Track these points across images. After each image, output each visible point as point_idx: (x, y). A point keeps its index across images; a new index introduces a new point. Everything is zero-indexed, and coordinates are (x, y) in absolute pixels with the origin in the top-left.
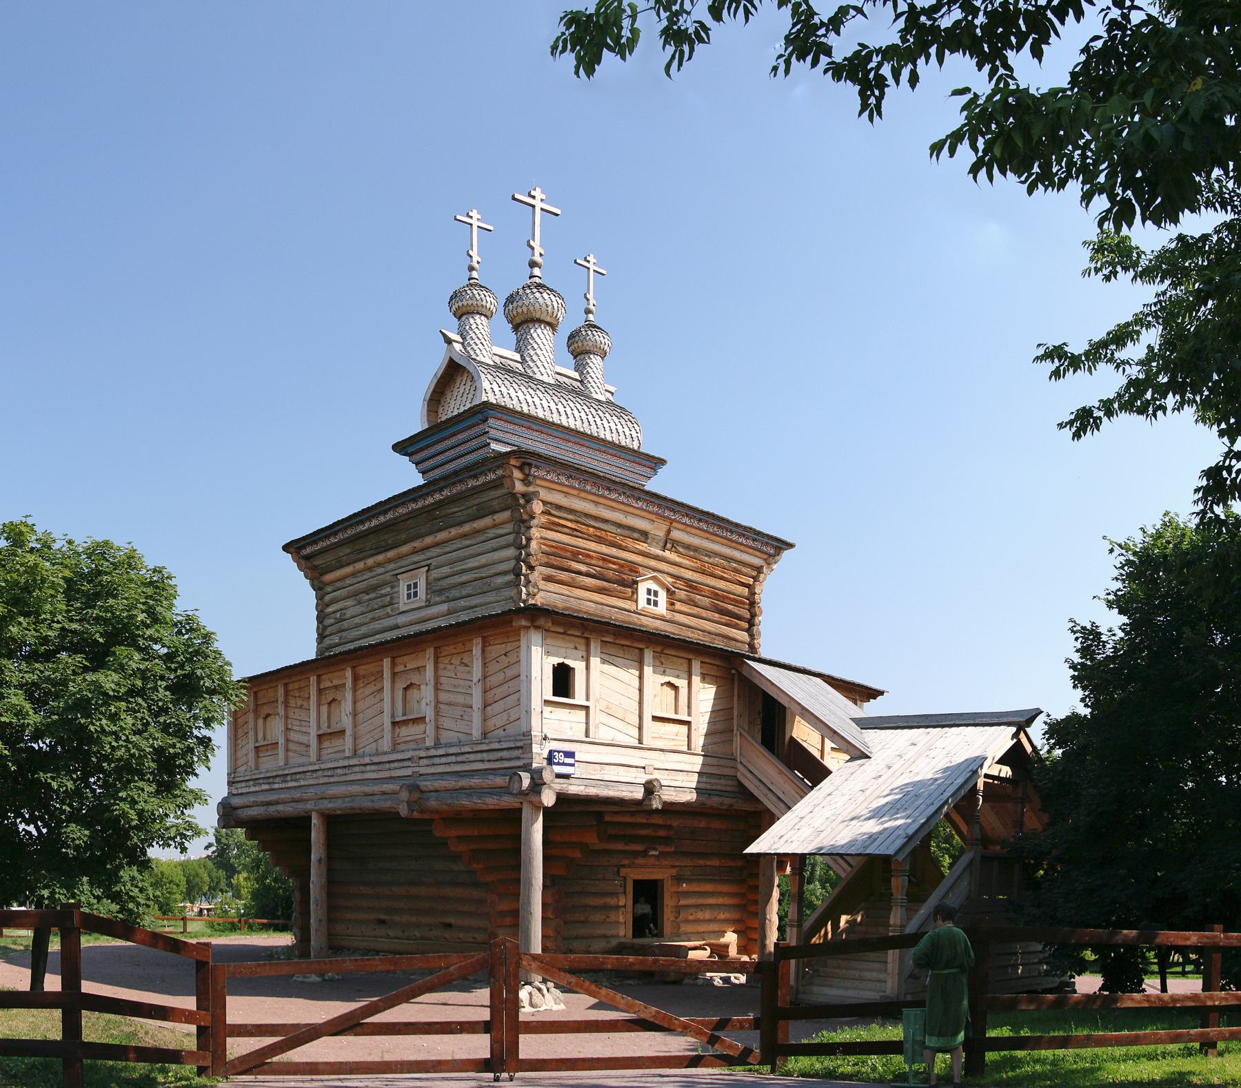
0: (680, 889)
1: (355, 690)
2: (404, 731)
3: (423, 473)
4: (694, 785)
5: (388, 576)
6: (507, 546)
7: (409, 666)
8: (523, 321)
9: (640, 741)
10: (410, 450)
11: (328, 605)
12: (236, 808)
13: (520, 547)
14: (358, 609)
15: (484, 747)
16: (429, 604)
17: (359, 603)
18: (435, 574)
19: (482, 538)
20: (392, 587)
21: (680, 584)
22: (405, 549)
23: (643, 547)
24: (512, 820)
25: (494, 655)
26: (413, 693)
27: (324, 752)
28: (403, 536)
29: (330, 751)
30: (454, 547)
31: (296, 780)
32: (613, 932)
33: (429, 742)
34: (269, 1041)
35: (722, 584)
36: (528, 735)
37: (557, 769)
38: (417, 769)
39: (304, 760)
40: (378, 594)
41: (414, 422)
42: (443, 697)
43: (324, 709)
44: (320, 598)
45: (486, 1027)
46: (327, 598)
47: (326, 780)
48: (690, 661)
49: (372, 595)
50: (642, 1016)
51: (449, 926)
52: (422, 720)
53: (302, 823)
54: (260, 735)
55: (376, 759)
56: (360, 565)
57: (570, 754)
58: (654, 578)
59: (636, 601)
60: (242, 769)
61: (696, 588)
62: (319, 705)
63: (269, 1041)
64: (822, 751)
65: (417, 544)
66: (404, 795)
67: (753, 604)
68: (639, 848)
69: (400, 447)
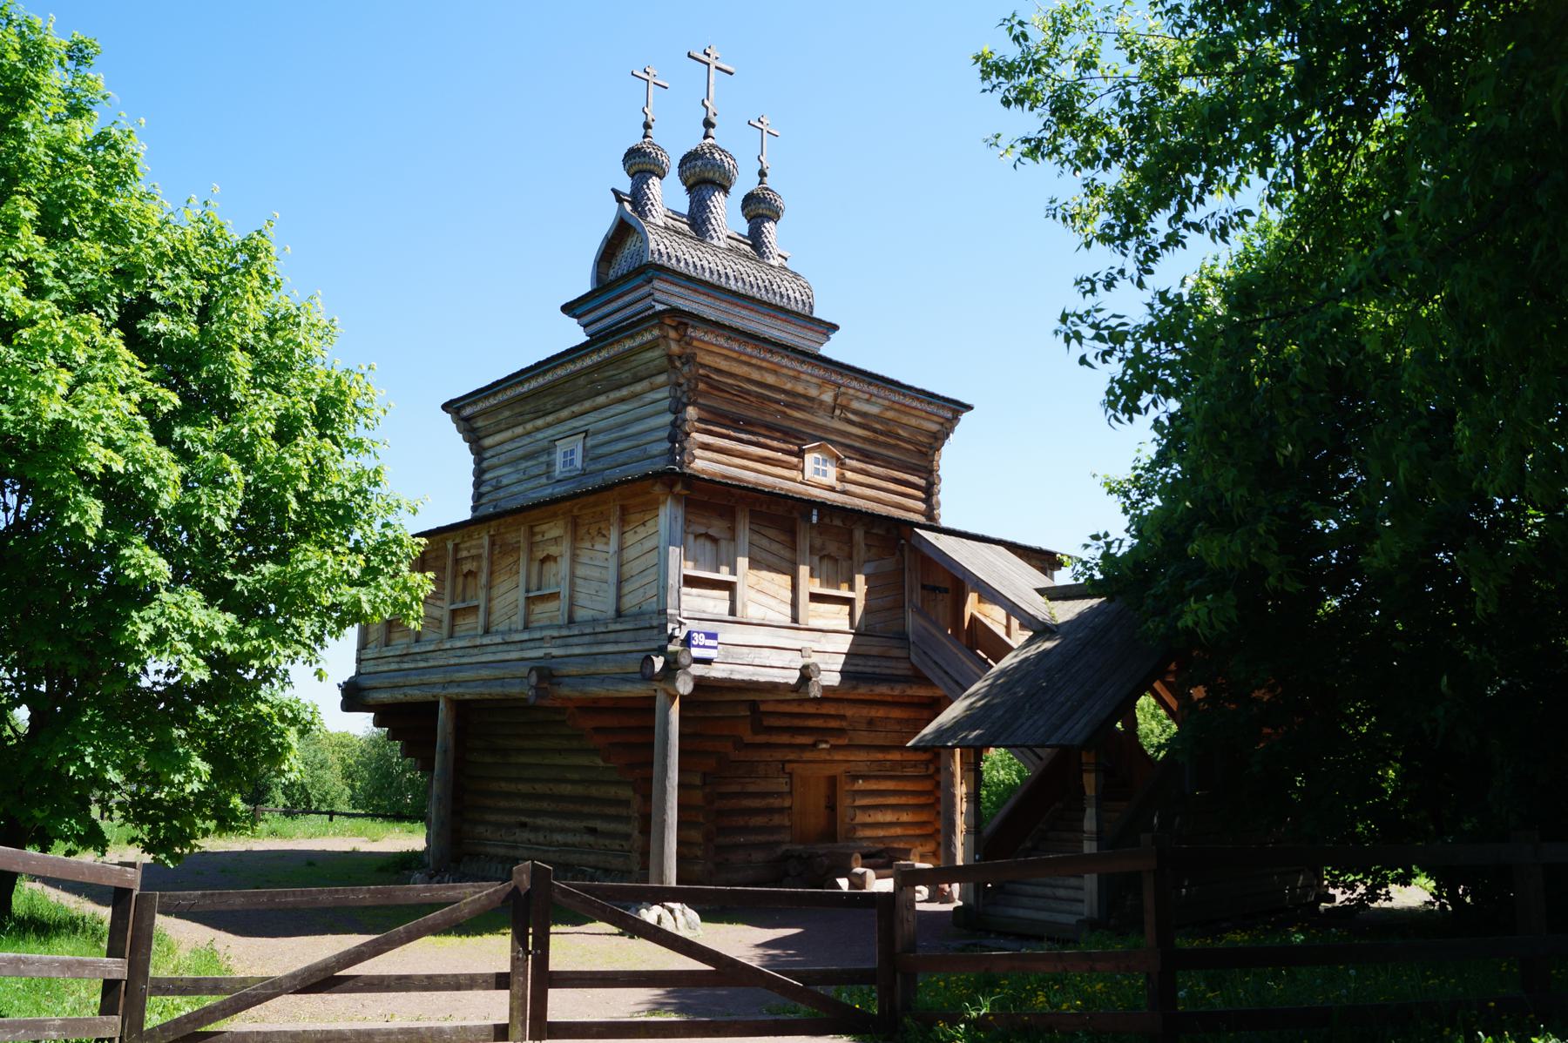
0: (856, 787)
1: (491, 563)
2: (539, 608)
4: (839, 668)
5: (545, 443)
9: (795, 619)
10: (578, 312)
14: (514, 478)
15: (618, 627)
17: (517, 471)
18: (590, 442)
20: (549, 454)
22: (565, 413)
26: (550, 568)
30: (612, 412)
31: (426, 660)
37: (695, 652)
41: (582, 285)
44: (478, 462)
45: (501, 981)
46: (485, 464)
47: (457, 661)
51: (592, 831)
52: (554, 596)
53: (430, 708)
56: (519, 430)
57: (713, 636)
59: (803, 471)
60: (372, 645)
62: (455, 577)
65: (576, 408)
69: (568, 309)
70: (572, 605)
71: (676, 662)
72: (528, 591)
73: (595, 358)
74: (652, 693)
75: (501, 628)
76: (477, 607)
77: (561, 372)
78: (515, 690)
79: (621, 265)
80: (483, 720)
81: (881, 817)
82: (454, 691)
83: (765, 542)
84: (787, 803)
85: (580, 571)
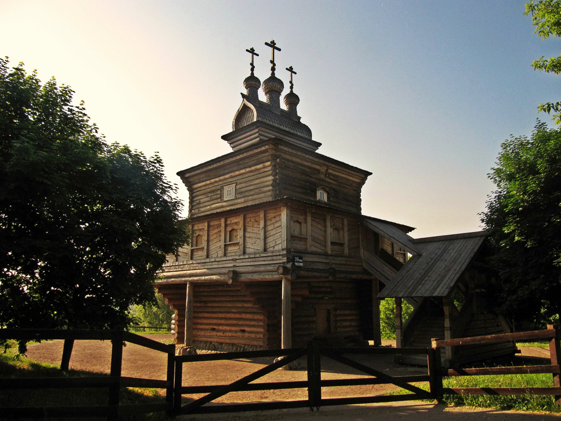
3: (233, 147)
6: (269, 175)
14: (207, 199)
15: (265, 255)
16: (236, 199)
17: (207, 197)
18: (238, 187)
22: (227, 176)
34: (202, 395)
40: (217, 193)
41: (229, 129)
46: (194, 195)
48: (343, 220)
50: (230, 351)
51: (243, 331)
53: (182, 286)
55: (217, 260)
56: (208, 182)
63: (202, 395)
65: (232, 174)
68: (320, 296)
69: (224, 137)
70: (244, 247)
72: (225, 242)
74: (280, 279)
76: (203, 248)
81: (344, 324)
83: (316, 224)
84: (314, 319)
85: (247, 235)
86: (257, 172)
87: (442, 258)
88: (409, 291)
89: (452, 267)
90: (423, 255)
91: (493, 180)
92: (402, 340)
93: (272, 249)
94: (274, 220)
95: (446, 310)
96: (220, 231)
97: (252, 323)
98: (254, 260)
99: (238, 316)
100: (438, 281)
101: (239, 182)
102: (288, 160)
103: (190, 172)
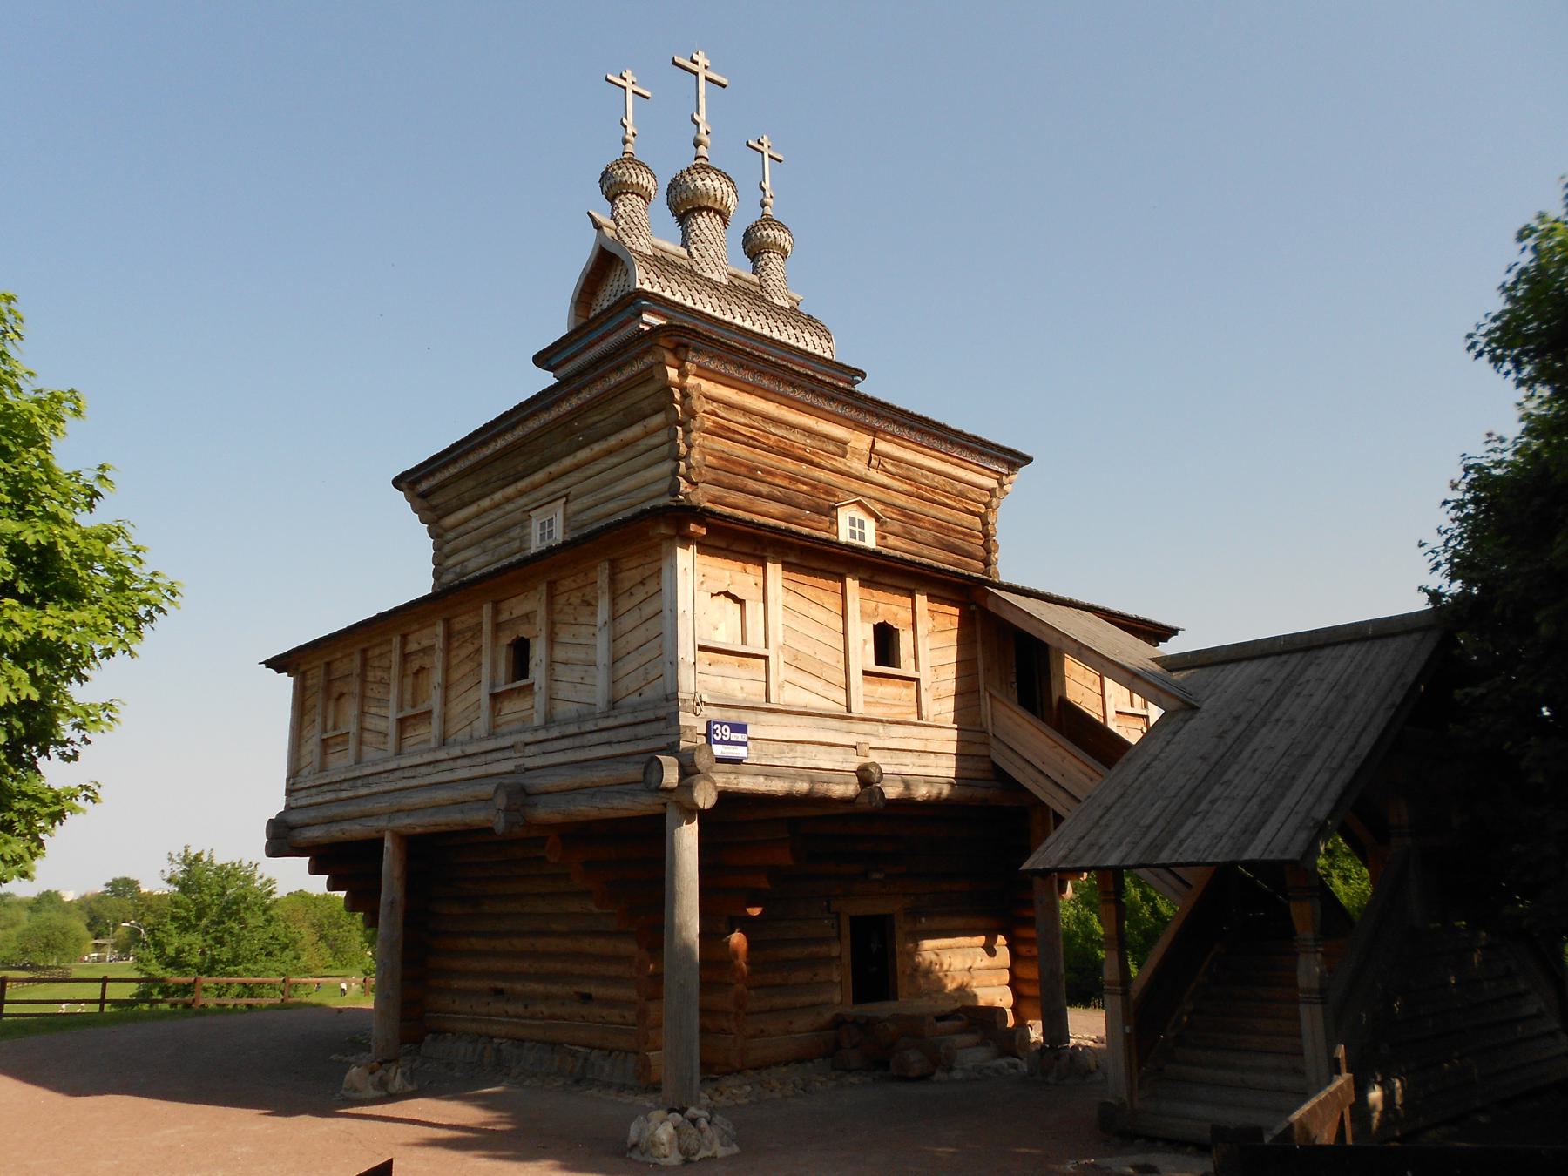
5: (518, 515)
7: (516, 613)
8: (686, 206)
10: (554, 362)
11: (448, 557)
12: (293, 828)
13: (677, 459)
18: (573, 507)
19: (632, 454)
20: (523, 527)
21: (890, 512)
22: (539, 477)
23: (837, 463)
24: (649, 839)
25: (627, 585)
27: (407, 743)
28: (536, 459)
29: (413, 741)
32: (823, 998)
33: (538, 720)
35: (944, 513)
36: (672, 697)
37: (718, 750)
38: (521, 761)
39: (380, 755)
42: (560, 654)
43: (409, 681)
44: (437, 548)
46: (447, 548)
49: (500, 541)
51: (586, 998)
53: (375, 845)
54: (330, 724)
55: (470, 750)
56: (486, 503)
57: (741, 728)
58: (859, 503)
60: (305, 772)
61: (912, 517)
62: (403, 676)
64: (1105, 717)
65: (553, 468)
66: (501, 801)
67: (987, 536)
69: (542, 359)
71: (693, 763)
73: (575, 402)
74: (659, 809)
75: (460, 737)
76: (429, 713)
77: (533, 424)
78: (477, 817)
79: (604, 301)
80: (430, 853)
82: (404, 822)
83: (802, 605)
86: (629, 453)
87: (1277, 714)
88: (1145, 842)
89: (1317, 746)
90: (1205, 706)
91: (1486, 357)
92: (1127, 1037)
93: (635, 698)
94: (640, 594)
95: (1303, 915)
96: (478, 651)
97: (613, 970)
98: (578, 741)
99: (569, 944)
100: (1263, 802)
101: (573, 491)
102: (730, 406)
103: (432, 474)
